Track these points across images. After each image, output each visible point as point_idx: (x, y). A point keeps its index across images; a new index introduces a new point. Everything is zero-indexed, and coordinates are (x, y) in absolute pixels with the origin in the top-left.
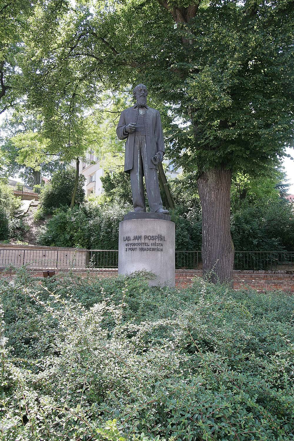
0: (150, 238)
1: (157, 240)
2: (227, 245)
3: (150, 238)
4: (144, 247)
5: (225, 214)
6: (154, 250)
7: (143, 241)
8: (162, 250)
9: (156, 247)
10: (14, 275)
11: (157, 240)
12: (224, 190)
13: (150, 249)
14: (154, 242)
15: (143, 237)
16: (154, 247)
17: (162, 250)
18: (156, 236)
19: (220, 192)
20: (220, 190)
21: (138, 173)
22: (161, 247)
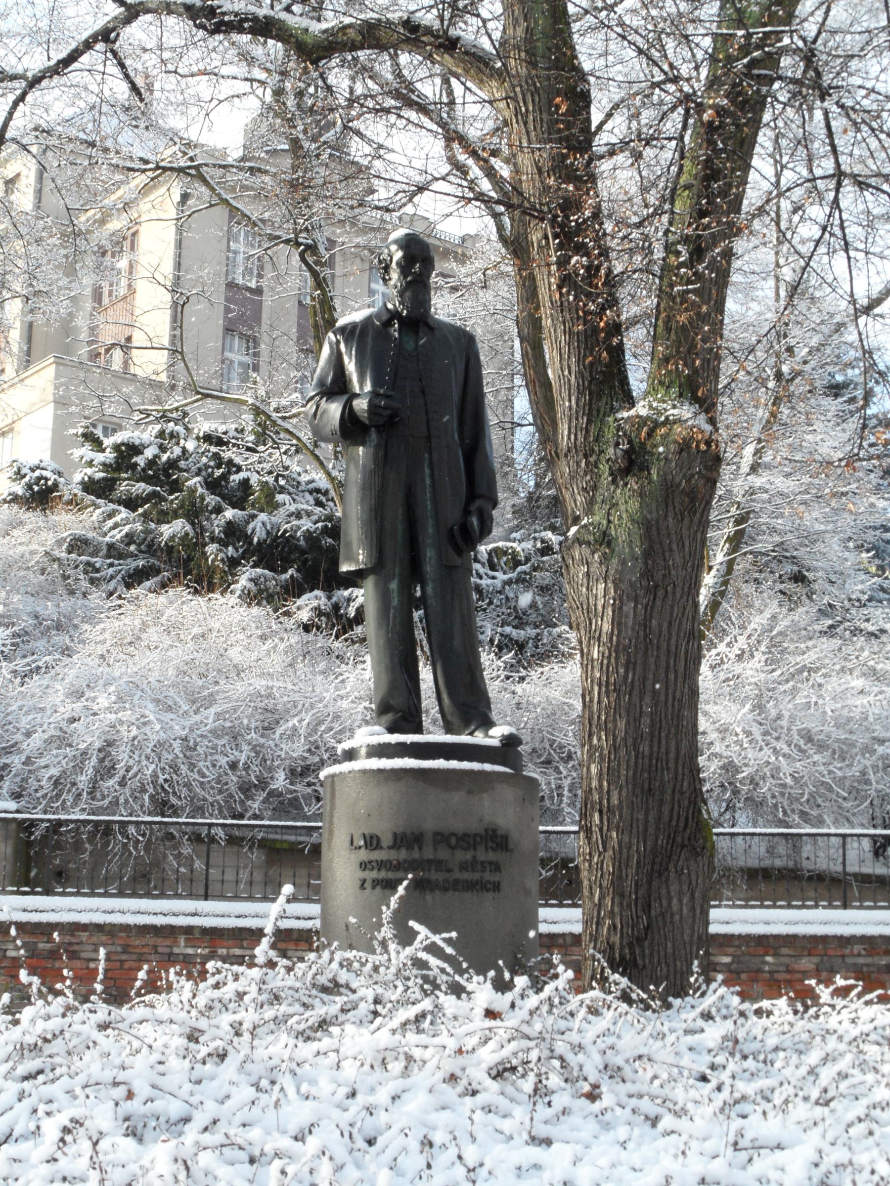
0: (453, 841)
1: (481, 849)
2: (686, 826)
3: (453, 841)
4: (435, 876)
5: (678, 695)
6: (470, 886)
7: (428, 853)
8: (496, 887)
9: (476, 876)
10: (84, 817)
11: (481, 849)
12: (678, 595)
13: (456, 886)
14: (469, 856)
15: (428, 839)
16: (467, 876)
17: (496, 887)
18: (475, 835)
19: (658, 603)
20: (660, 593)
21: (586, 883)
22: (495, 877)
